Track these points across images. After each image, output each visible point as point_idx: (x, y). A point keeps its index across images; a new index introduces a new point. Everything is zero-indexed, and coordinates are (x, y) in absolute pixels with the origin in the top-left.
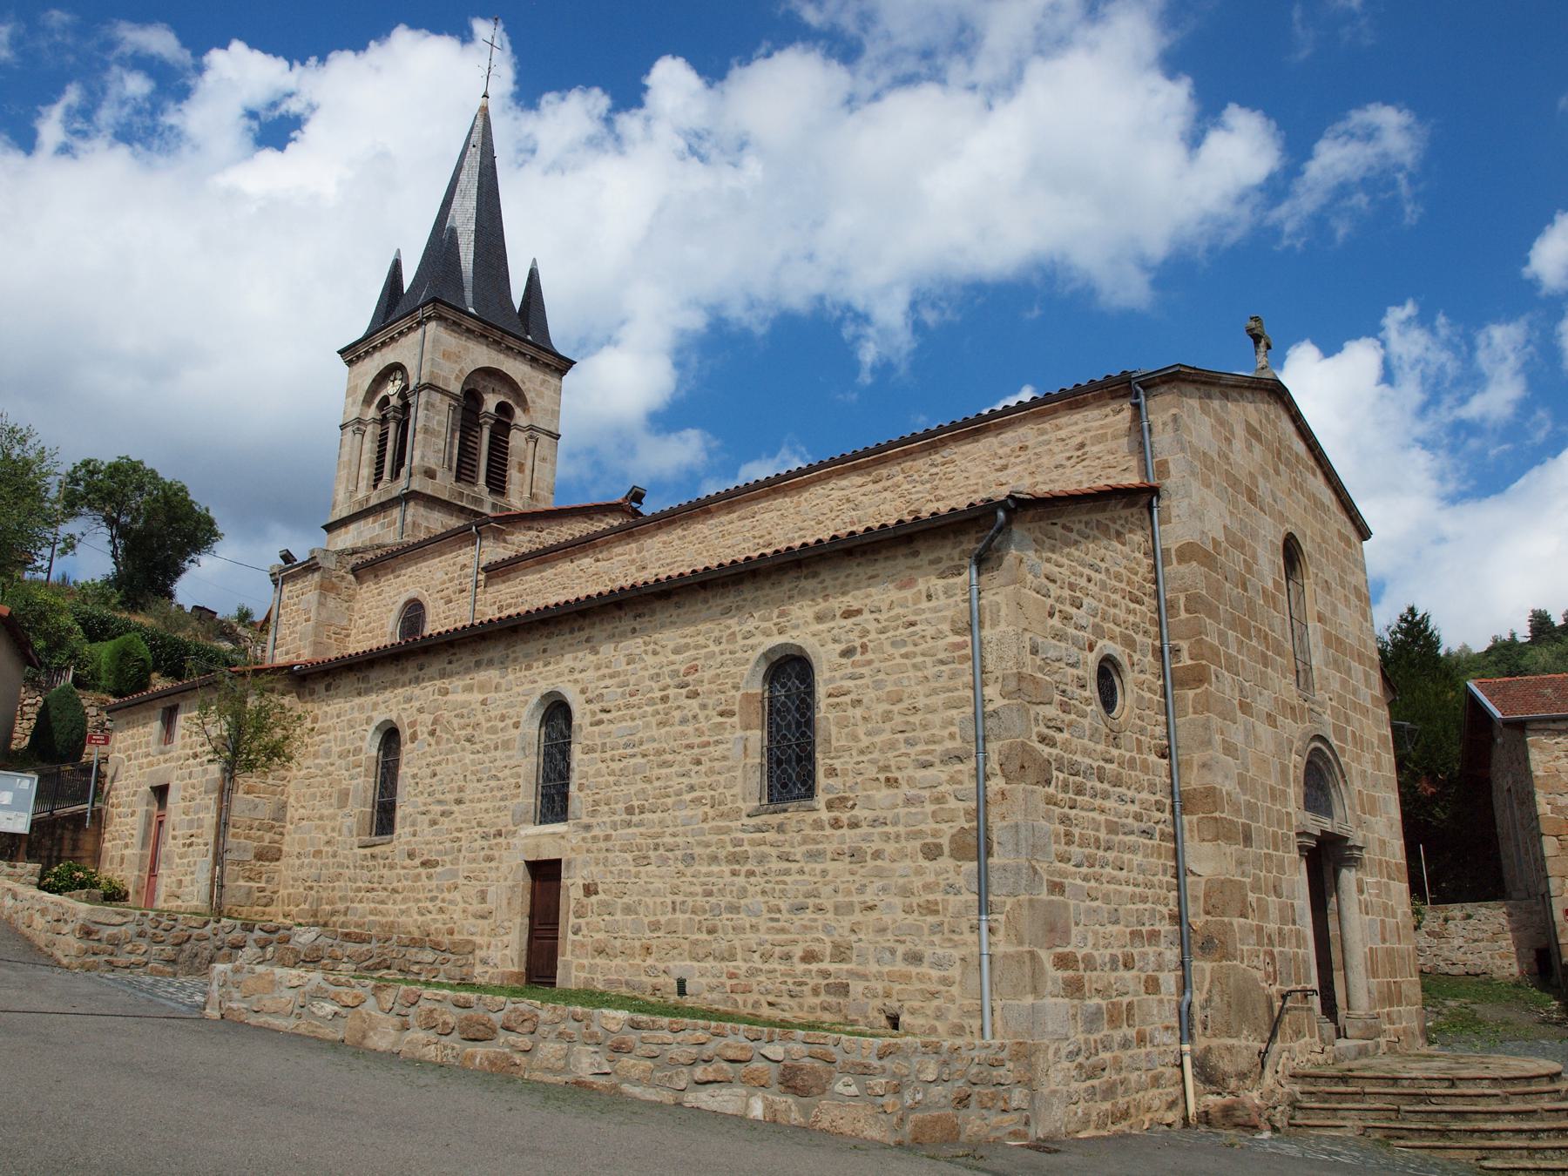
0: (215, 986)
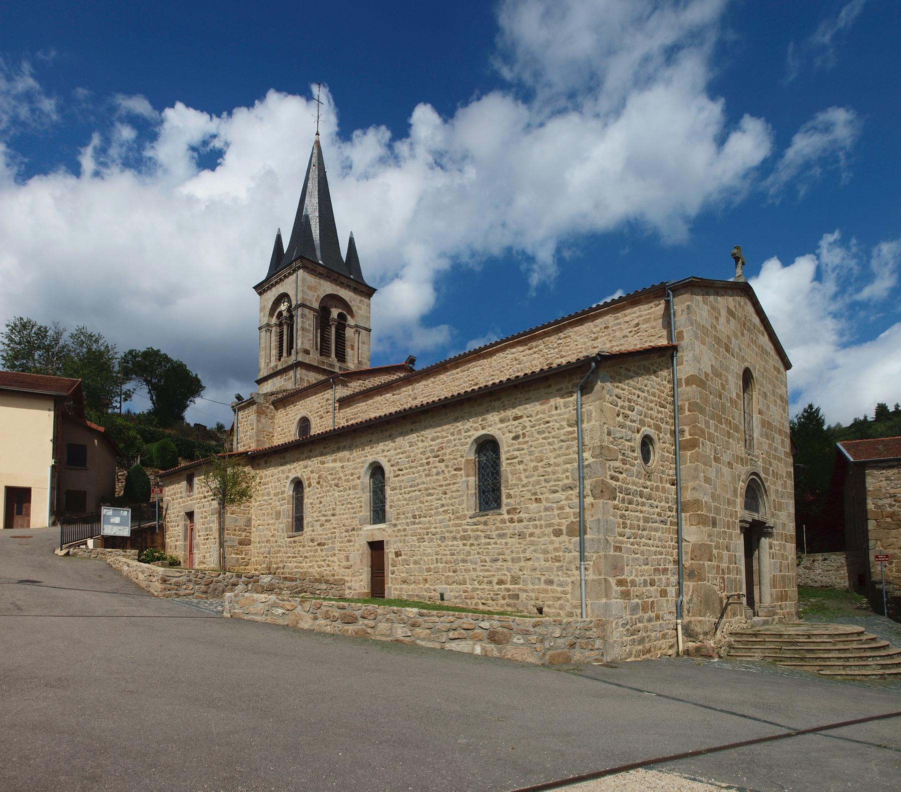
0: (227, 603)
